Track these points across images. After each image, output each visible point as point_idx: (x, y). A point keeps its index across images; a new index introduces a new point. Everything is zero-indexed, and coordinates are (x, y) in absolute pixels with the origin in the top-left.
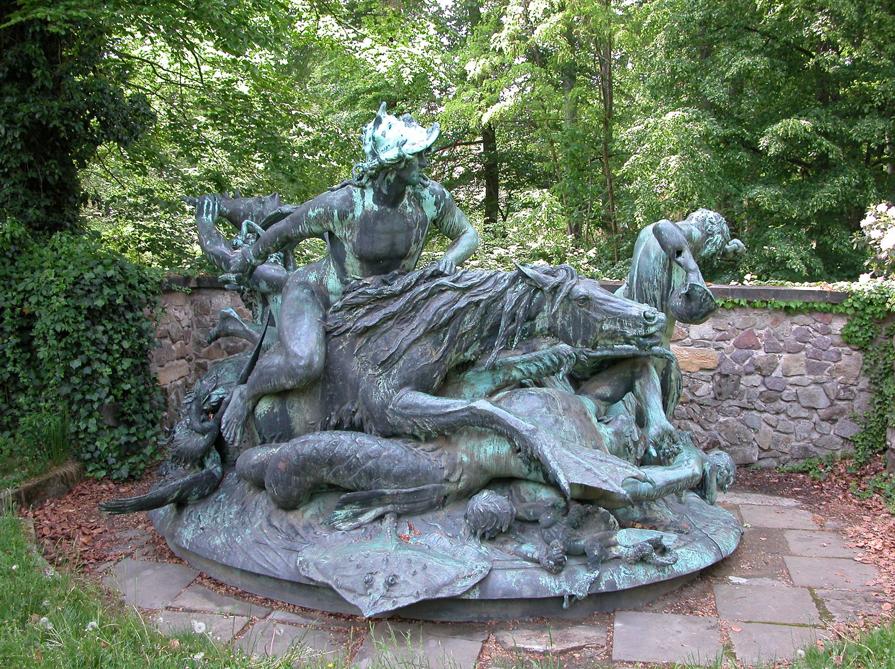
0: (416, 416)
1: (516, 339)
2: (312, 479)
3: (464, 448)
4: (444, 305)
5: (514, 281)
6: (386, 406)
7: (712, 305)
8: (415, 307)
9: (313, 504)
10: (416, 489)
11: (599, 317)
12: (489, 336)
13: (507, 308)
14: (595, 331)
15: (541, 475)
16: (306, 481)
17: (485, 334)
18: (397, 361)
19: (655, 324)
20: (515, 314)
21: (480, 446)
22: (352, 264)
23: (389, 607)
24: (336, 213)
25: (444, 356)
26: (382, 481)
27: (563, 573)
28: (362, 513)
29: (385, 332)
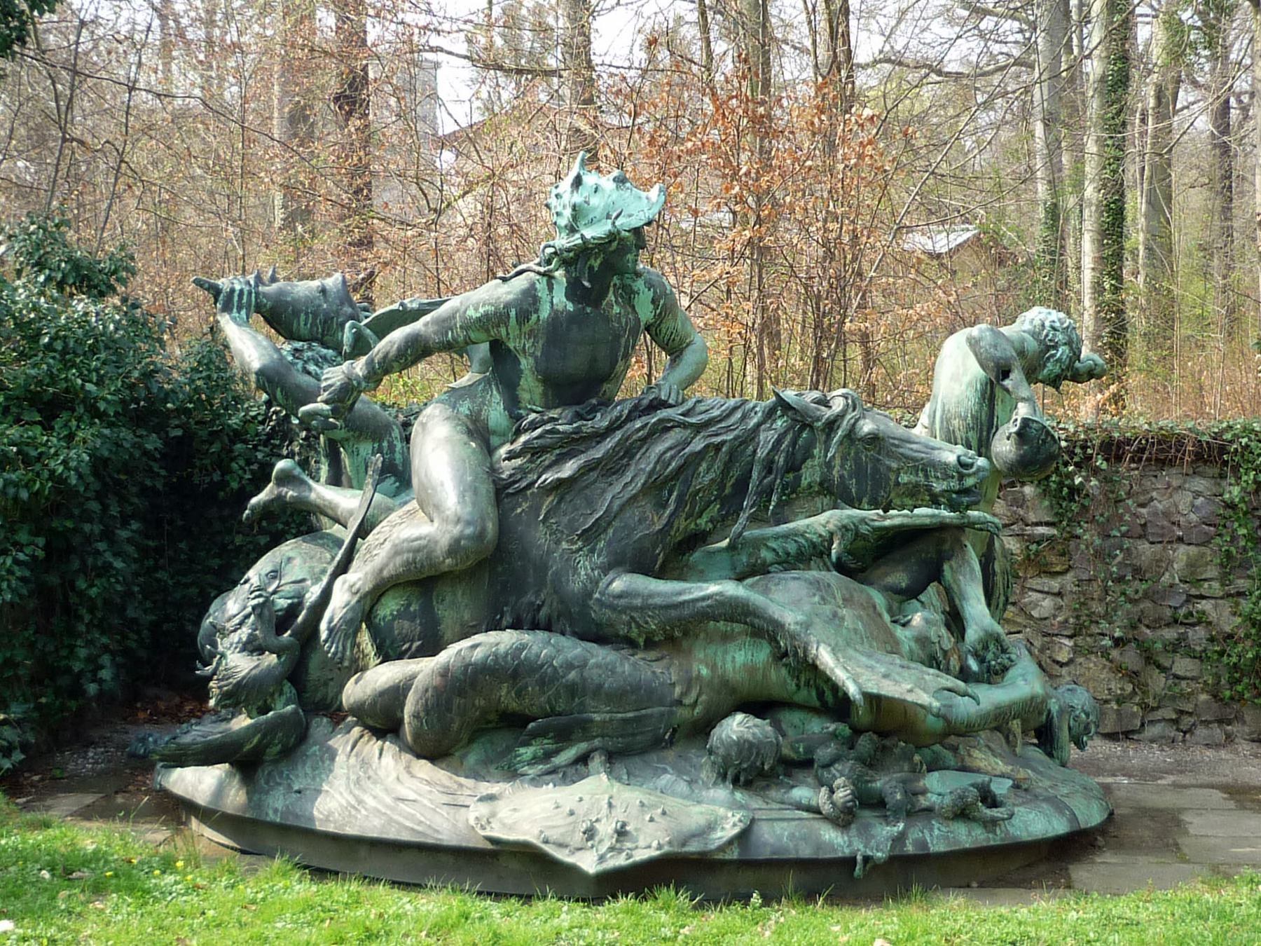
0: (635, 608)
1: (774, 498)
2: (482, 702)
3: (701, 655)
4: (670, 448)
5: (770, 414)
6: (589, 595)
7: (1055, 449)
8: (627, 452)
9: (475, 745)
10: (636, 714)
11: (894, 465)
12: (732, 495)
13: (761, 453)
14: (887, 484)
15: (814, 693)
16: (474, 705)
17: (727, 491)
18: (605, 530)
19: (974, 473)
20: (772, 462)
21: (726, 652)
22: (530, 387)
23: (620, 861)
24: (513, 313)
25: (669, 523)
26: (589, 701)
27: (853, 826)
28: (557, 752)
29: (586, 487)
